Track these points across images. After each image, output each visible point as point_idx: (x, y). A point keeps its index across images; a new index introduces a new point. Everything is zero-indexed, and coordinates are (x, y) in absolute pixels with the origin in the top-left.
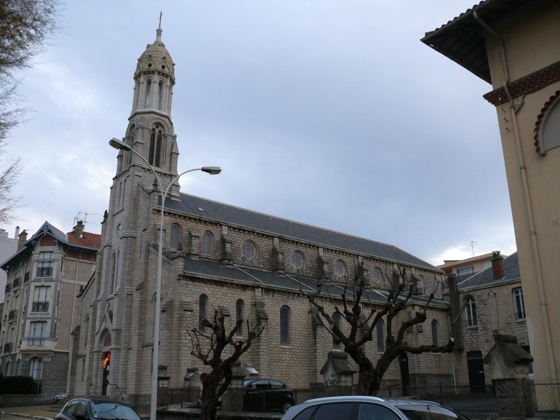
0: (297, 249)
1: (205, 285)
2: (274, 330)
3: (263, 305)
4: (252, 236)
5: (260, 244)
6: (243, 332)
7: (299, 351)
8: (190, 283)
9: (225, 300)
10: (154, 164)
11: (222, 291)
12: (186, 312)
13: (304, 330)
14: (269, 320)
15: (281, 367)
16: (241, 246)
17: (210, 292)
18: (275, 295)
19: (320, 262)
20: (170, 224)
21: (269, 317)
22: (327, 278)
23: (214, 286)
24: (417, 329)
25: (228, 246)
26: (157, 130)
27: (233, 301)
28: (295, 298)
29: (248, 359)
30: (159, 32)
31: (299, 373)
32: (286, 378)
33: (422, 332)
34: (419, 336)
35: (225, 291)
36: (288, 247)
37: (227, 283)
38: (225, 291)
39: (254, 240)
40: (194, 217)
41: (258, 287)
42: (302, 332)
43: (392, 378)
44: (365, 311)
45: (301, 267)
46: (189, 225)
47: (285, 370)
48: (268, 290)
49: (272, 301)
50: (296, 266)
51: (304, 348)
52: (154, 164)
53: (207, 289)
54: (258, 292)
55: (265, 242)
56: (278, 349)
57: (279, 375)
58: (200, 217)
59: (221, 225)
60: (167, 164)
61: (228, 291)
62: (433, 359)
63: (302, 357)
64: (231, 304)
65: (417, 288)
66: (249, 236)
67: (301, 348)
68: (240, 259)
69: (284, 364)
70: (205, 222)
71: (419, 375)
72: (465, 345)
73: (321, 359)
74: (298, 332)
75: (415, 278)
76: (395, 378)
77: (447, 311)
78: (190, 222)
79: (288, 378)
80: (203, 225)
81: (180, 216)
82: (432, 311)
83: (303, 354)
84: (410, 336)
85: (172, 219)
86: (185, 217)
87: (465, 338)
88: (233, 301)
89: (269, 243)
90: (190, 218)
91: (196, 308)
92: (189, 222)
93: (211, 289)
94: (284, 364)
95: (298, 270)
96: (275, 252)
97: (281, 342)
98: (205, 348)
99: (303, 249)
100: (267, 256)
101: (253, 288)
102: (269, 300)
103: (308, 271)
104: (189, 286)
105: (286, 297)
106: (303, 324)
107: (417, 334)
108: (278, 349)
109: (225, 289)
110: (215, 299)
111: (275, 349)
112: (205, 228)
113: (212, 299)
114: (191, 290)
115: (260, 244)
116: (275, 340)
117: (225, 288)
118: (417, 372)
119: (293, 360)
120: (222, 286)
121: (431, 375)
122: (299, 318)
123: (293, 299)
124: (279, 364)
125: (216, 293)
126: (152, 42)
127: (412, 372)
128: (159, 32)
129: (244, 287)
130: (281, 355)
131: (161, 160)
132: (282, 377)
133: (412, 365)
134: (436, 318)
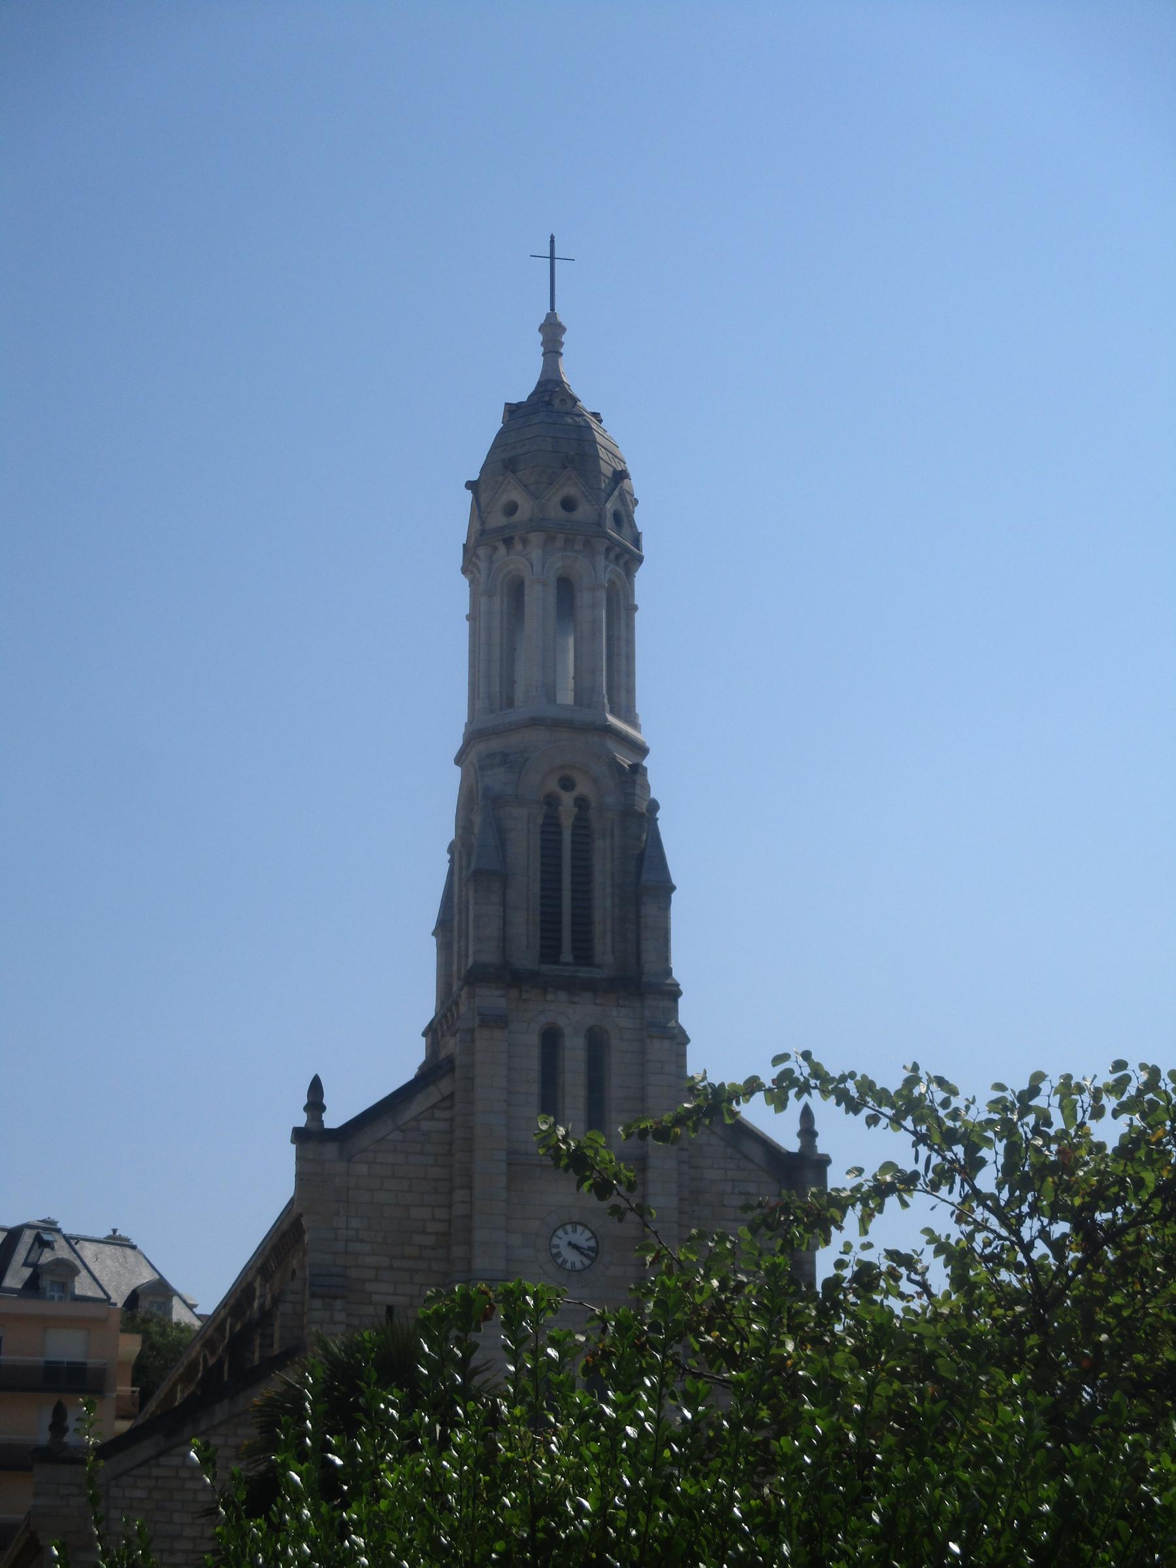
10: (567, 956)
26: (567, 799)
30: (552, 334)
52: (567, 956)
126: (522, 392)
128: (552, 334)
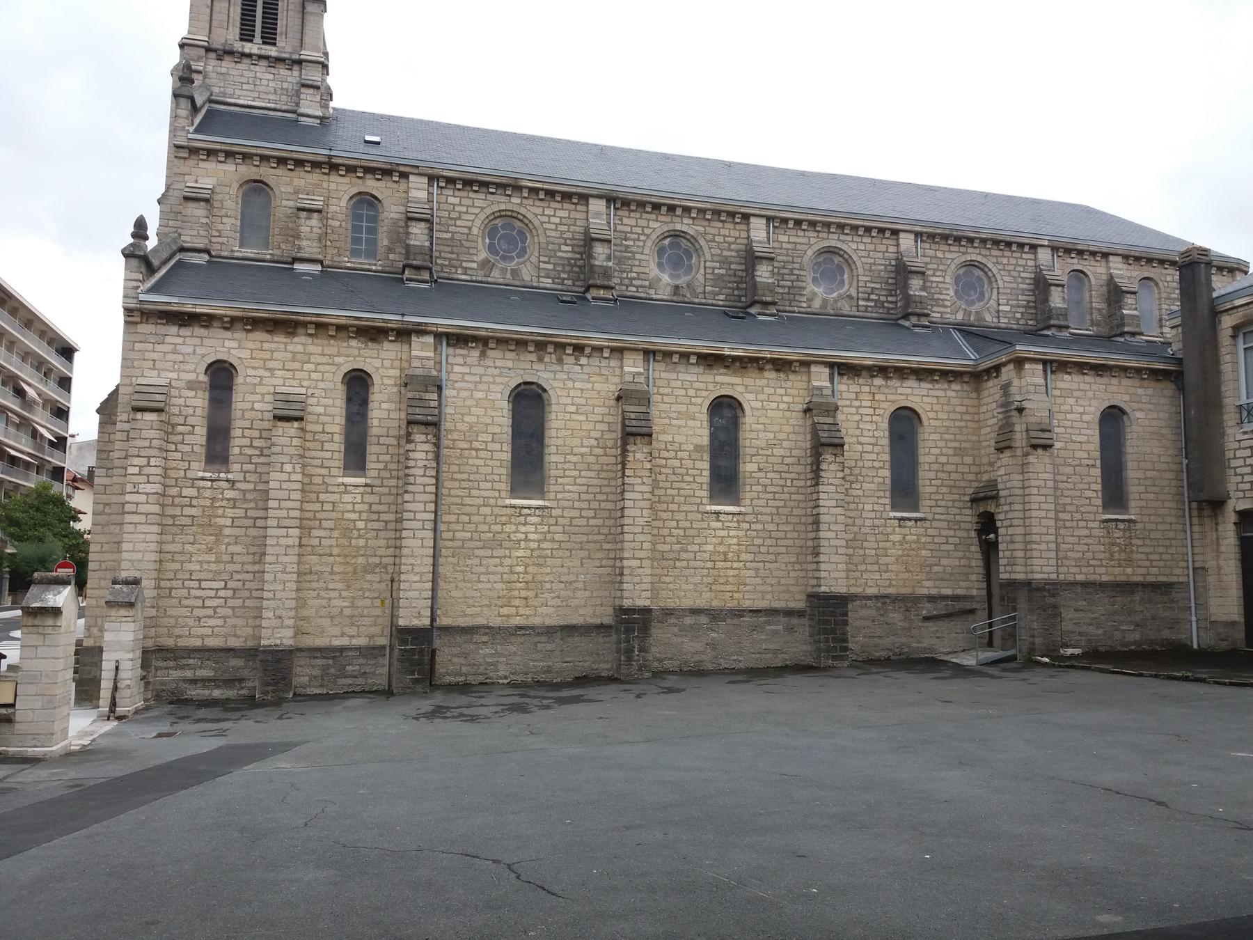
0: (671, 227)
1: (228, 334)
2: (482, 454)
3: (832, 410)
4: (516, 200)
5: (545, 219)
6: (369, 465)
7: (576, 513)
8: (174, 329)
9: (299, 375)
11: (290, 348)
12: (139, 416)
13: (599, 451)
14: (846, 447)
15: (507, 562)
16: (475, 231)
17: (245, 354)
18: (489, 352)
19: (902, 272)
20: (235, 186)
21: (846, 440)
22: (766, 304)
23: (260, 335)
24: (1029, 438)
25: (600, 250)
27: (328, 376)
28: (567, 359)
29: (382, 543)
31: (573, 578)
32: (523, 593)
33: (1046, 447)
34: (1031, 459)
35: (300, 348)
36: (643, 223)
37: (305, 325)
38: (300, 348)
39: (523, 211)
40: (310, 158)
41: (421, 331)
42: (591, 459)
43: (948, 592)
44: (843, 388)
45: (687, 278)
46: (297, 182)
47: (521, 569)
48: (844, 369)
49: (480, 370)
50: (671, 276)
51: (595, 505)
52: (258, 39)
53: (234, 344)
54: (422, 349)
55: (560, 213)
56: (496, 510)
57: (500, 586)
58: (330, 157)
59: (746, 217)
60: (294, 34)
61: (311, 349)
62: (1097, 532)
63: (586, 530)
64: (321, 385)
65: (1123, 317)
66: (503, 199)
67: (585, 505)
68: (474, 265)
69: (520, 553)
70: (351, 169)
71: (1027, 584)
72: (1231, 487)
73: (639, 538)
74: (575, 459)
75: (1117, 288)
76: (959, 592)
77: (1171, 374)
78: (303, 174)
79: (531, 594)
80: (347, 180)
81: (264, 158)
82: (1105, 380)
83: (592, 522)
84: (1005, 461)
85: (243, 169)
86: (282, 161)
87: (1234, 463)
88: (328, 376)
89: (577, 215)
90: (299, 163)
91: (199, 402)
92: (299, 172)
93: (250, 345)
94: (520, 553)
95: (677, 287)
96: (902, 272)
97: (711, 497)
98: (223, 516)
99: (684, 225)
100: (566, 251)
101: (404, 334)
102: (466, 370)
103: (708, 289)
104: (168, 339)
105: (476, 353)
106: (598, 435)
107: (1027, 454)
108: (496, 510)
109: (299, 343)
110: (261, 372)
111: (486, 510)
112: (352, 185)
113: (251, 372)
114: (175, 352)
115: (545, 219)
116: (489, 485)
117: (300, 339)
118: (1021, 576)
119: (553, 540)
120: (293, 334)
121: (1074, 584)
122: (583, 418)
123: (560, 361)
124: (501, 552)
125: (267, 355)
127: (1006, 576)
129: (373, 334)
130: (507, 528)
131: (280, 28)
132: (510, 590)
133: (1008, 554)
134: (1120, 400)
